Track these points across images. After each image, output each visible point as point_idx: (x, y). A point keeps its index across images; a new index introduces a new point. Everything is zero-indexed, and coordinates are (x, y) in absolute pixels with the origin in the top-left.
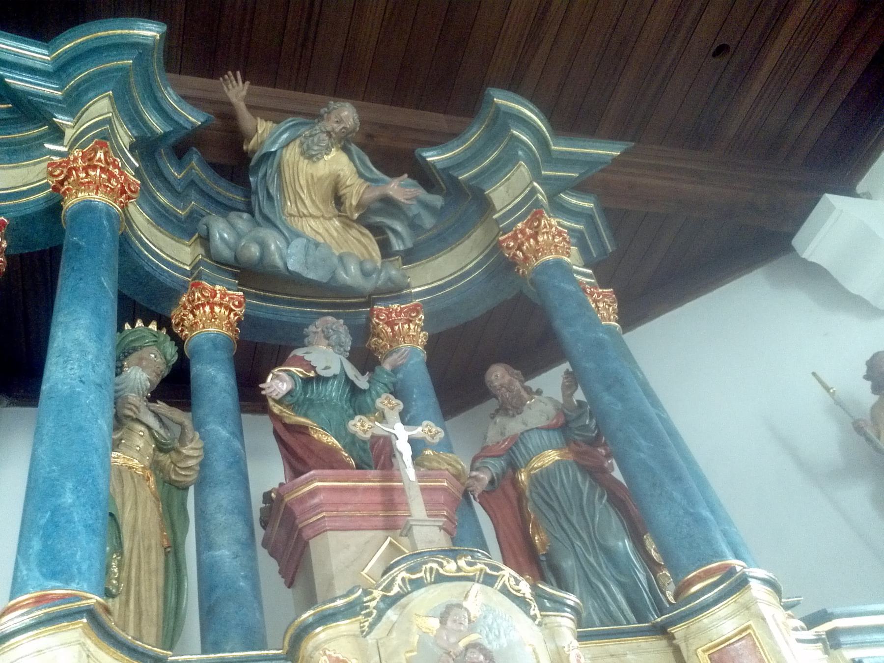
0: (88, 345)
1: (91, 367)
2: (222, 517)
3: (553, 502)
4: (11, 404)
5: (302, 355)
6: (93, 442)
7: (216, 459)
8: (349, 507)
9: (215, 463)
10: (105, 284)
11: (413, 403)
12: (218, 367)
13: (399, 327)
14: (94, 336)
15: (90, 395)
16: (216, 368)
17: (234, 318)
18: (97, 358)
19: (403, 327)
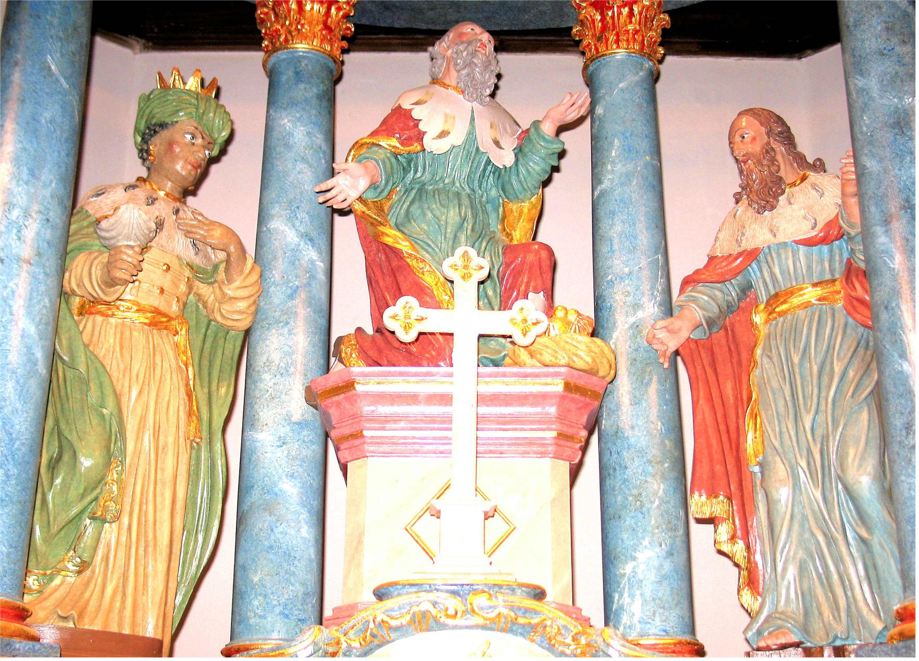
0: (15, 191)
1: (15, 231)
2: (270, 379)
3: (536, 612)
4: (146, 48)
5: (410, 107)
6: (8, 362)
7: (274, 283)
8: (402, 424)
9: (272, 289)
10: (53, 67)
11: (609, 167)
12: (298, 115)
13: (613, 12)
14: (25, 175)
15: (8, 282)
16: (295, 116)
17: (336, 16)
18: (27, 214)
19: (620, 13)
